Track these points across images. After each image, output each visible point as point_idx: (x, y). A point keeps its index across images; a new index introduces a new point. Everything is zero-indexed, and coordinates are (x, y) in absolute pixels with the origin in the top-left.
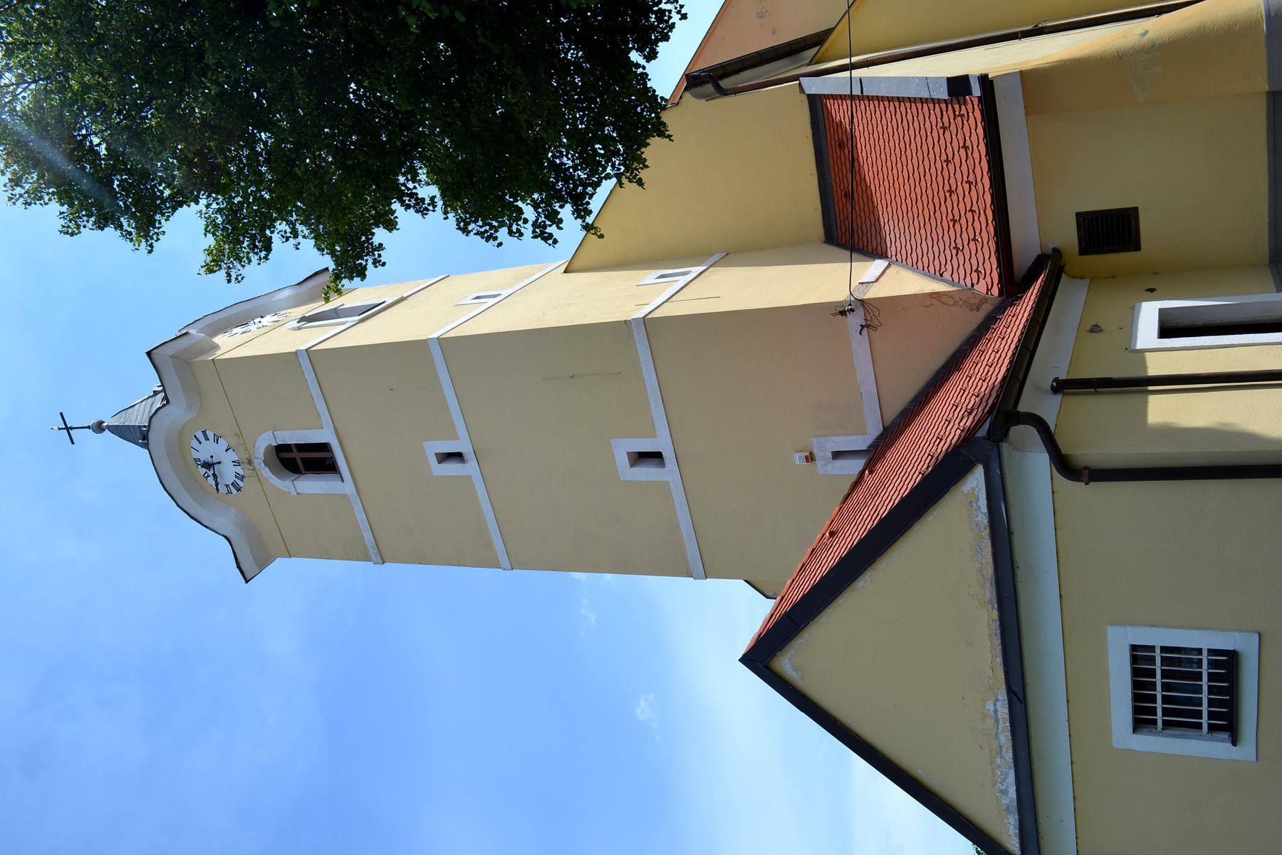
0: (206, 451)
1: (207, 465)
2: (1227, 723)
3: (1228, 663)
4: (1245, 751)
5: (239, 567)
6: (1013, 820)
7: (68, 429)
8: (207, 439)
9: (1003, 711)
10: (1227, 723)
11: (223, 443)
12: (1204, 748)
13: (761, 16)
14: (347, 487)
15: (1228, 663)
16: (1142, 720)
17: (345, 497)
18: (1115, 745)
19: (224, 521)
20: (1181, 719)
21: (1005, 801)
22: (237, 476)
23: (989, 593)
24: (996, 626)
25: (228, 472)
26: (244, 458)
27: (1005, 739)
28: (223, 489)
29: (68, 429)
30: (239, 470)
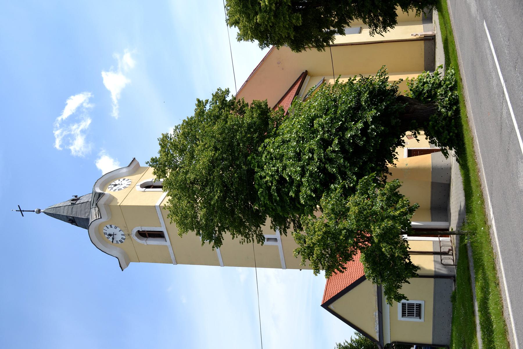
0: (111, 231)
1: (110, 235)
2: (419, 315)
3: (419, 306)
4: (422, 320)
5: (121, 266)
6: (377, 335)
7: (21, 211)
8: (111, 227)
9: (377, 314)
10: (419, 315)
11: (118, 229)
12: (415, 320)
13: (278, 63)
14: (168, 243)
15: (419, 306)
16: (404, 315)
17: (166, 246)
18: (286, 44)
19: (116, 252)
20: (411, 314)
21: (376, 331)
22: (122, 238)
23: (376, 294)
24: (377, 300)
25: (118, 237)
26: (127, 233)
27: (377, 319)
28: (115, 242)
29: (21, 211)
30: (124, 237)
